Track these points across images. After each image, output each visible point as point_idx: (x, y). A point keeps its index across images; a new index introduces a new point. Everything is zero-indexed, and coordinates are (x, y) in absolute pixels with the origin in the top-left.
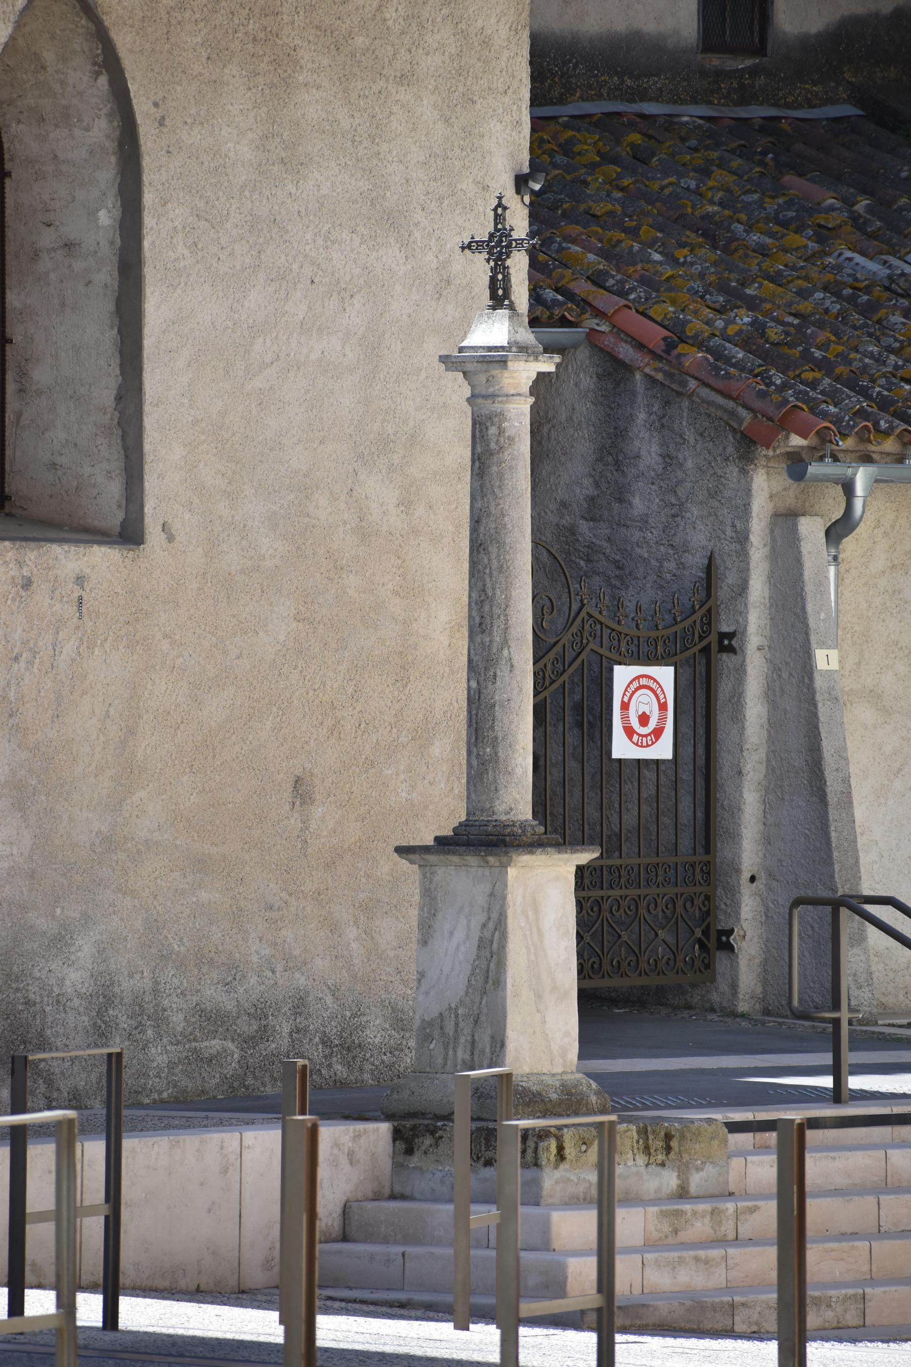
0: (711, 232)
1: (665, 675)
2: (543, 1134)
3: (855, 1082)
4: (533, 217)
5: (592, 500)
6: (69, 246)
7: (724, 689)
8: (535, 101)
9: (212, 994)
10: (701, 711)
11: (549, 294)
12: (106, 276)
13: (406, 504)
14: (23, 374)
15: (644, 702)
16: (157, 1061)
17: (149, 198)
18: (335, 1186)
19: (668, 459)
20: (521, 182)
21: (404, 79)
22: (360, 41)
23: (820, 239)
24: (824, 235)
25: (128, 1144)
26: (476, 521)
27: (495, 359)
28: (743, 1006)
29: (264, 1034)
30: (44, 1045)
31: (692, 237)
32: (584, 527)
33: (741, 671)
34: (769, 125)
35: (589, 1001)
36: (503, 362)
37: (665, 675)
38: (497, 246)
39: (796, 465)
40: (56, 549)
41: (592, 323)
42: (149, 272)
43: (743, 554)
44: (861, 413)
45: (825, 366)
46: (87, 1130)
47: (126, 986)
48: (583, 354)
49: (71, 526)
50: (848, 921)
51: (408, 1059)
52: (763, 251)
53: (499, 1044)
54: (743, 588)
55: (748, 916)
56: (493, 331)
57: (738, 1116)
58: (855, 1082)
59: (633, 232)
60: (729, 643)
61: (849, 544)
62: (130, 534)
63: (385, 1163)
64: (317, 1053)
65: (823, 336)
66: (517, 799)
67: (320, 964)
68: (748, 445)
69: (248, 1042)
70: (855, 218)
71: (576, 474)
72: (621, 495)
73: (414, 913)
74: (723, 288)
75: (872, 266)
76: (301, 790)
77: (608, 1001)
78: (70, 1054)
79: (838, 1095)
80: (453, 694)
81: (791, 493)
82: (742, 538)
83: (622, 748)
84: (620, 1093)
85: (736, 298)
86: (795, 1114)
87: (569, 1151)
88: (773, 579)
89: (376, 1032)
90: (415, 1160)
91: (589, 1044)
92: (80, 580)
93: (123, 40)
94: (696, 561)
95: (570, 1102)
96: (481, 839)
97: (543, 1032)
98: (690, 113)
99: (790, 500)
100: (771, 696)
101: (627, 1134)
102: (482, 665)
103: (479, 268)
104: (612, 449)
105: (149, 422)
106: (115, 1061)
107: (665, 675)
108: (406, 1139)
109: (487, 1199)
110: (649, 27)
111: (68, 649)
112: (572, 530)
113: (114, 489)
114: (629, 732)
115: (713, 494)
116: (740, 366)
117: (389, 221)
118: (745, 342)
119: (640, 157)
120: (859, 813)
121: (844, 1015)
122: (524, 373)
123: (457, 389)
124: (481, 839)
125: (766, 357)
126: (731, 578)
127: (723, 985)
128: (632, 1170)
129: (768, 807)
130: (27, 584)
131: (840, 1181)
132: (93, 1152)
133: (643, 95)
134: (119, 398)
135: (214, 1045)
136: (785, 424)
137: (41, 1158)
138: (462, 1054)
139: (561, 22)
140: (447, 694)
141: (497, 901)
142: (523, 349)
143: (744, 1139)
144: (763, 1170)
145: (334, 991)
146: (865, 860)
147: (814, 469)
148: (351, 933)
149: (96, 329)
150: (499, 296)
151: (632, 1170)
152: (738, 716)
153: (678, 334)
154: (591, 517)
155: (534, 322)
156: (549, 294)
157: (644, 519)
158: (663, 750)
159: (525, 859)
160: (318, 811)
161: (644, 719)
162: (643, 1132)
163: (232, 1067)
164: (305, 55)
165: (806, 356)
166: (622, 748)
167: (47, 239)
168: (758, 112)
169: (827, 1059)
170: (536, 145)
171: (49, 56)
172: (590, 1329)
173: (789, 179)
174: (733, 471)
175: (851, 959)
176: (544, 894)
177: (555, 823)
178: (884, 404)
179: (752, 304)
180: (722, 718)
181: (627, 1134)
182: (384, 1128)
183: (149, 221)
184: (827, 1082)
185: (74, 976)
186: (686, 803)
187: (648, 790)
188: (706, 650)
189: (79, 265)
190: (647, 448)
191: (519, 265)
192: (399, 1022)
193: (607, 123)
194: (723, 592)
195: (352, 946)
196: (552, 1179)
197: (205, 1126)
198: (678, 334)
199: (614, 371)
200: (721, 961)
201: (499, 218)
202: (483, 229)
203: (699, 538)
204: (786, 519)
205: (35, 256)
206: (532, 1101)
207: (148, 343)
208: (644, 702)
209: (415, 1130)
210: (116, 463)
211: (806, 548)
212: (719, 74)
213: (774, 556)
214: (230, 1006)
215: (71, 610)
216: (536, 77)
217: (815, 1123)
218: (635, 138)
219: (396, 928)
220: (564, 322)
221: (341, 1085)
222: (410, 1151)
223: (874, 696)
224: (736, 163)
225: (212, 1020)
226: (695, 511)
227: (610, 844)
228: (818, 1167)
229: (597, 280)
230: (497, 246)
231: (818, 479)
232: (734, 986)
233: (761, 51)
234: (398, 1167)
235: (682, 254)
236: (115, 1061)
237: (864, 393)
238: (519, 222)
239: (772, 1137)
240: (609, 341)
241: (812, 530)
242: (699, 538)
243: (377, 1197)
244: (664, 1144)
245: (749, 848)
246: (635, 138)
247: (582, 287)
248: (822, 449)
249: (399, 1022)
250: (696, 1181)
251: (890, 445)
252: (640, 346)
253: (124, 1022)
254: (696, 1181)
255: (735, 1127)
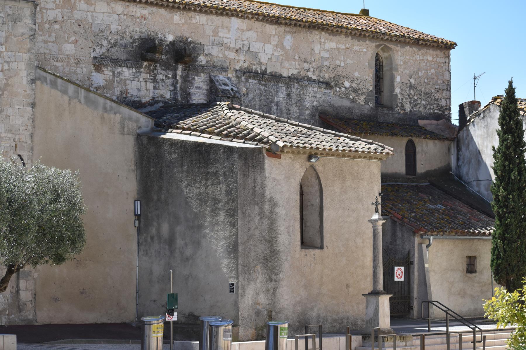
0: (408, 202)
1: (402, 268)
2: (385, 337)
3: (431, 329)
4: (382, 199)
5: (391, 242)
6: (312, 205)
7: (411, 270)
8: (382, 182)
9: (335, 317)
10: (408, 273)
11: (384, 211)
12: (318, 209)
13: (363, 242)
14: (305, 224)
15: (399, 272)
16: (327, 327)
17: (324, 197)
18: (354, 345)
19: (402, 235)
20: (380, 194)
21: (362, 179)
22: (355, 174)
23: (424, 203)
24: (425, 202)
25: (323, 339)
26: (374, 245)
27: (376, 221)
28: (415, 318)
29: (343, 322)
30: (310, 324)
31: (405, 202)
32: (390, 246)
33: (414, 267)
34: (417, 186)
35: (391, 317)
36: (377, 221)
37: (402, 268)
38: (376, 204)
39: (422, 236)
40: (311, 250)
41: (391, 215)
42: (324, 208)
43: (414, 249)
44: (431, 228)
45: (426, 221)
46: (317, 337)
47: (322, 315)
48: (389, 220)
49: (314, 247)
50: (430, 305)
51: (364, 326)
52: (416, 204)
53: (378, 324)
54: (414, 255)
55: (415, 304)
56: (376, 217)
57: (414, 334)
58: (431, 329)
59: (396, 202)
60: (412, 263)
61: (430, 248)
62: (321, 248)
63: (361, 342)
64: (351, 325)
65: (425, 217)
66: (380, 287)
67: (351, 312)
68: (414, 233)
69: (340, 324)
70: (429, 199)
71: (389, 237)
72: (395, 241)
73: (365, 304)
74: (410, 210)
75: (432, 207)
76: (348, 286)
77: (394, 317)
78: (314, 325)
79: (429, 331)
80: (371, 271)
81: (421, 241)
82: (414, 247)
83: (396, 279)
84: (396, 330)
85: (412, 211)
86: (423, 334)
87: (389, 340)
88: (418, 254)
89: (359, 322)
90: (366, 341)
91: (392, 323)
92: (314, 255)
93: (320, 175)
94: (407, 251)
95: (389, 332)
96: (375, 293)
97: (385, 321)
98: (405, 184)
99: (421, 241)
100: (418, 271)
101: (398, 337)
102: (375, 267)
103: (374, 207)
104: (394, 234)
105: (324, 231)
106: (321, 327)
107: (402, 268)
108: (364, 338)
109: (377, 347)
110: (398, 172)
111: (312, 265)
112: (388, 246)
113: (319, 241)
114: (397, 277)
115: (409, 241)
116: (413, 221)
117: (360, 200)
118: (413, 218)
119: (397, 191)
120: (432, 288)
121: (430, 319)
122: (381, 223)
123: (371, 225)
124: (375, 293)
125: (416, 220)
126: (412, 253)
127: (411, 315)
128: (398, 342)
129: (418, 288)
130: (306, 255)
131: (429, 343)
132: (318, 340)
133: (397, 182)
134: (320, 227)
135: (335, 324)
136: (420, 230)
137: (310, 341)
138: (372, 325)
139: (385, 171)
140: (370, 271)
141: (378, 302)
142: (380, 219)
143: (415, 337)
144: (418, 342)
145: (353, 316)
146: (433, 295)
147: (424, 237)
148: (355, 307)
149: (316, 217)
150: (377, 211)
151: (398, 342)
152: (413, 274)
153: (404, 217)
154: (391, 244)
155: (382, 215)
156: (384, 211)
157: (399, 245)
158: (402, 279)
159: (382, 296)
160: (350, 289)
161: (399, 275)
162: (400, 337)
163: (338, 328)
164: (347, 176)
165: (423, 220)
166: (396, 279)
167: (309, 204)
168: (415, 184)
169: (427, 325)
170: (382, 189)
171: (309, 177)
172: (449, 52)
173: (420, 194)
174: (412, 237)
175: (431, 310)
176: (385, 302)
177: (387, 290)
178: (434, 227)
179: (414, 212)
180: (411, 274)
181: (398, 337)
182: (361, 336)
183: (324, 201)
184: (427, 329)
185: (314, 314)
186: (406, 287)
187: (400, 285)
188: (408, 264)
189: (314, 208)
190: (399, 234)
191: (380, 207)
192: (363, 321)
193: (392, 186)
194: (411, 255)
195: (355, 309)
196: (386, 344)
197: (334, 336)
198: (404, 217)
199: (394, 222)
200: (411, 311)
201: (376, 200)
202: (374, 201)
203: (407, 247)
204: (420, 244)
205: (307, 206)
206: (383, 332)
207: (324, 219)
208: (399, 272)
209: (366, 337)
210: (319, 237)
211: (423, 249)
212: (409, 178)
213: (419, 250)
214: (337, 318)
215: (313, 259)
216: (382, 179)
217: (426, 335)
218: (396, 188)
219: (362, 307)
220: (386, 215)
221: (354, 330)
222: (365, 340)
223: (434, 271)
224: (412, 191)
225: (335, 320)
226: (406, 243)
227: (395, 294)
228: (426, 341)
229: (391, 209)
230: (376, 204)
231: (426, 238)
232: (413, 315)
233: (415, 175)
234: (363, 342)
235: (404, 205)
236: (321, 327)
237: (432, 225)
238: (379, 200)
239: (419, 337)
240: (393, 218)
241: (424, 246)
242: (407, 247)
243: (360, 347)
244: (403, 338)
245: (415, 294)
246: (396, 188)
247: (389, 210)
248: (425, 234)
249: (363, 321)
250: (408, 344)
251: (436, 233)
252: (398, 218)
253: (322, 321)
254: (408, 344)
255: (414, 336)
